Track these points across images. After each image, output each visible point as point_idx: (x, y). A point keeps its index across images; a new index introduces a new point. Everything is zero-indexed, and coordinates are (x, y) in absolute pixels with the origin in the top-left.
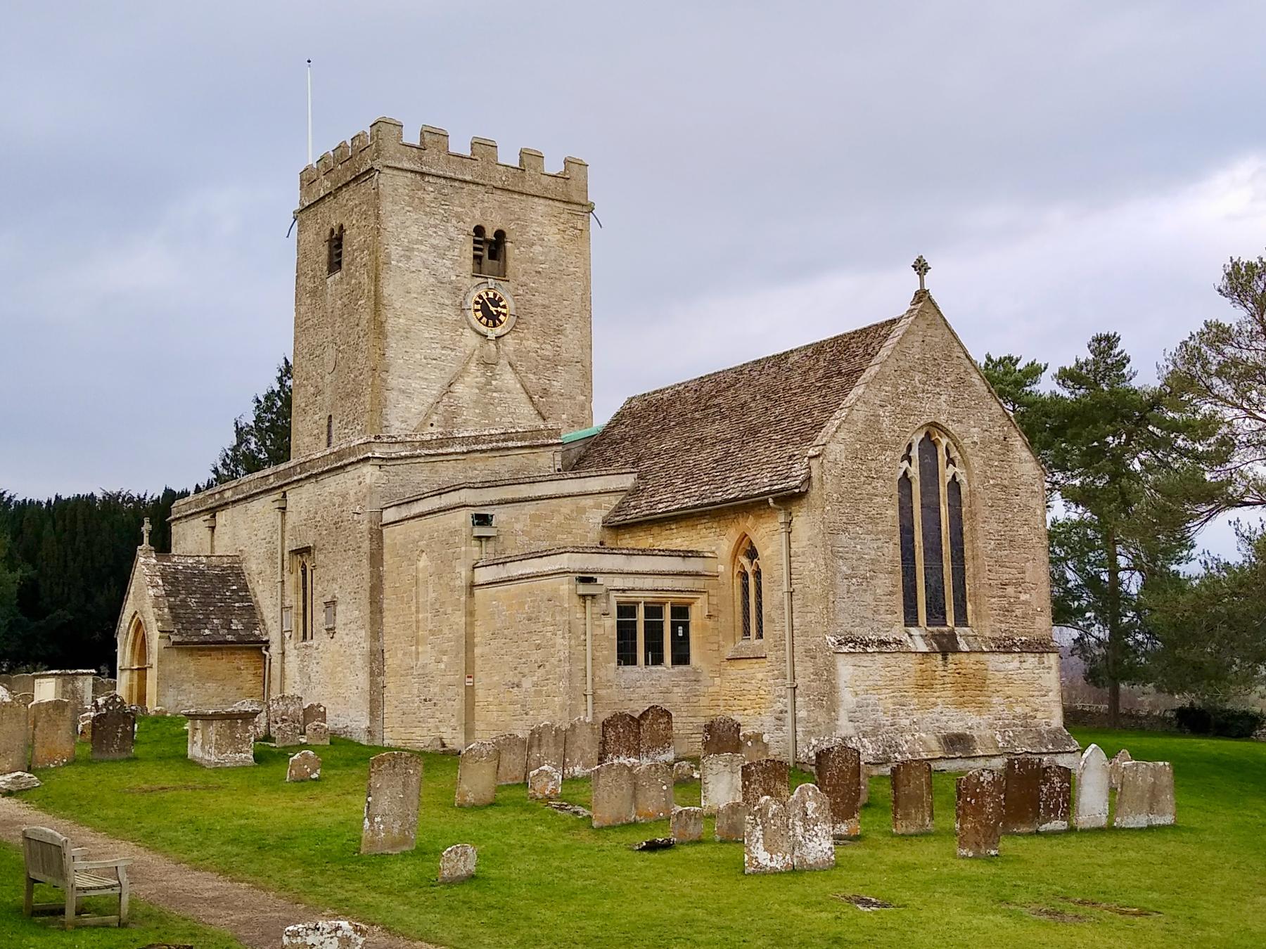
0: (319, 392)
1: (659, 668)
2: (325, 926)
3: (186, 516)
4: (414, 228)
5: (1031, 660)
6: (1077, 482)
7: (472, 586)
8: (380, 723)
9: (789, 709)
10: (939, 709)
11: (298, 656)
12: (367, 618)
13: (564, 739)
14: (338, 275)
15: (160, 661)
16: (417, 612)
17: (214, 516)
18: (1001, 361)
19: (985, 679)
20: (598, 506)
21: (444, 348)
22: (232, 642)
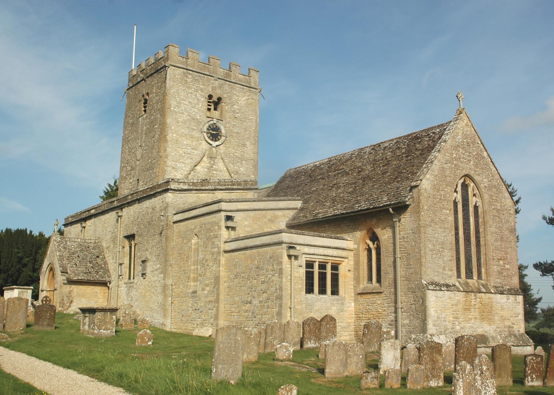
0: (133, 169)
5: (512, 297)
20: (284, 216)
21: (192, 149)
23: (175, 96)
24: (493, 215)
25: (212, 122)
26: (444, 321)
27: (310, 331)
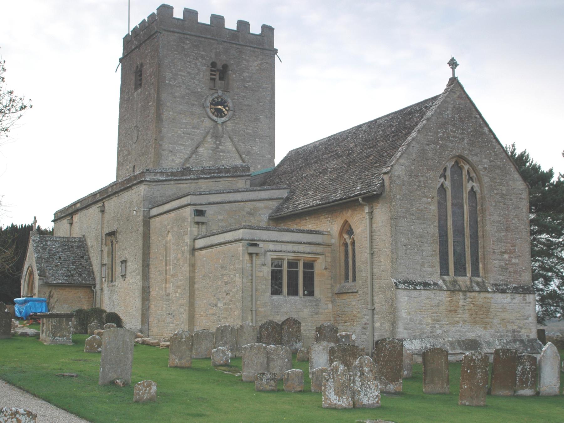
0: (129, 154)
5: (518, 297)
7: (194, 250)
9: (370, 322)
12: (141, 269)
13: (236, 333)
14: (139, 90)
15: (39, 292)
17: (72, 218)
20: (267, 208)
21: (193, 128)
23: (171, 66)
24: (495, 201)
25: (216, 95)
26: (419, 324)
27: (269, 335)
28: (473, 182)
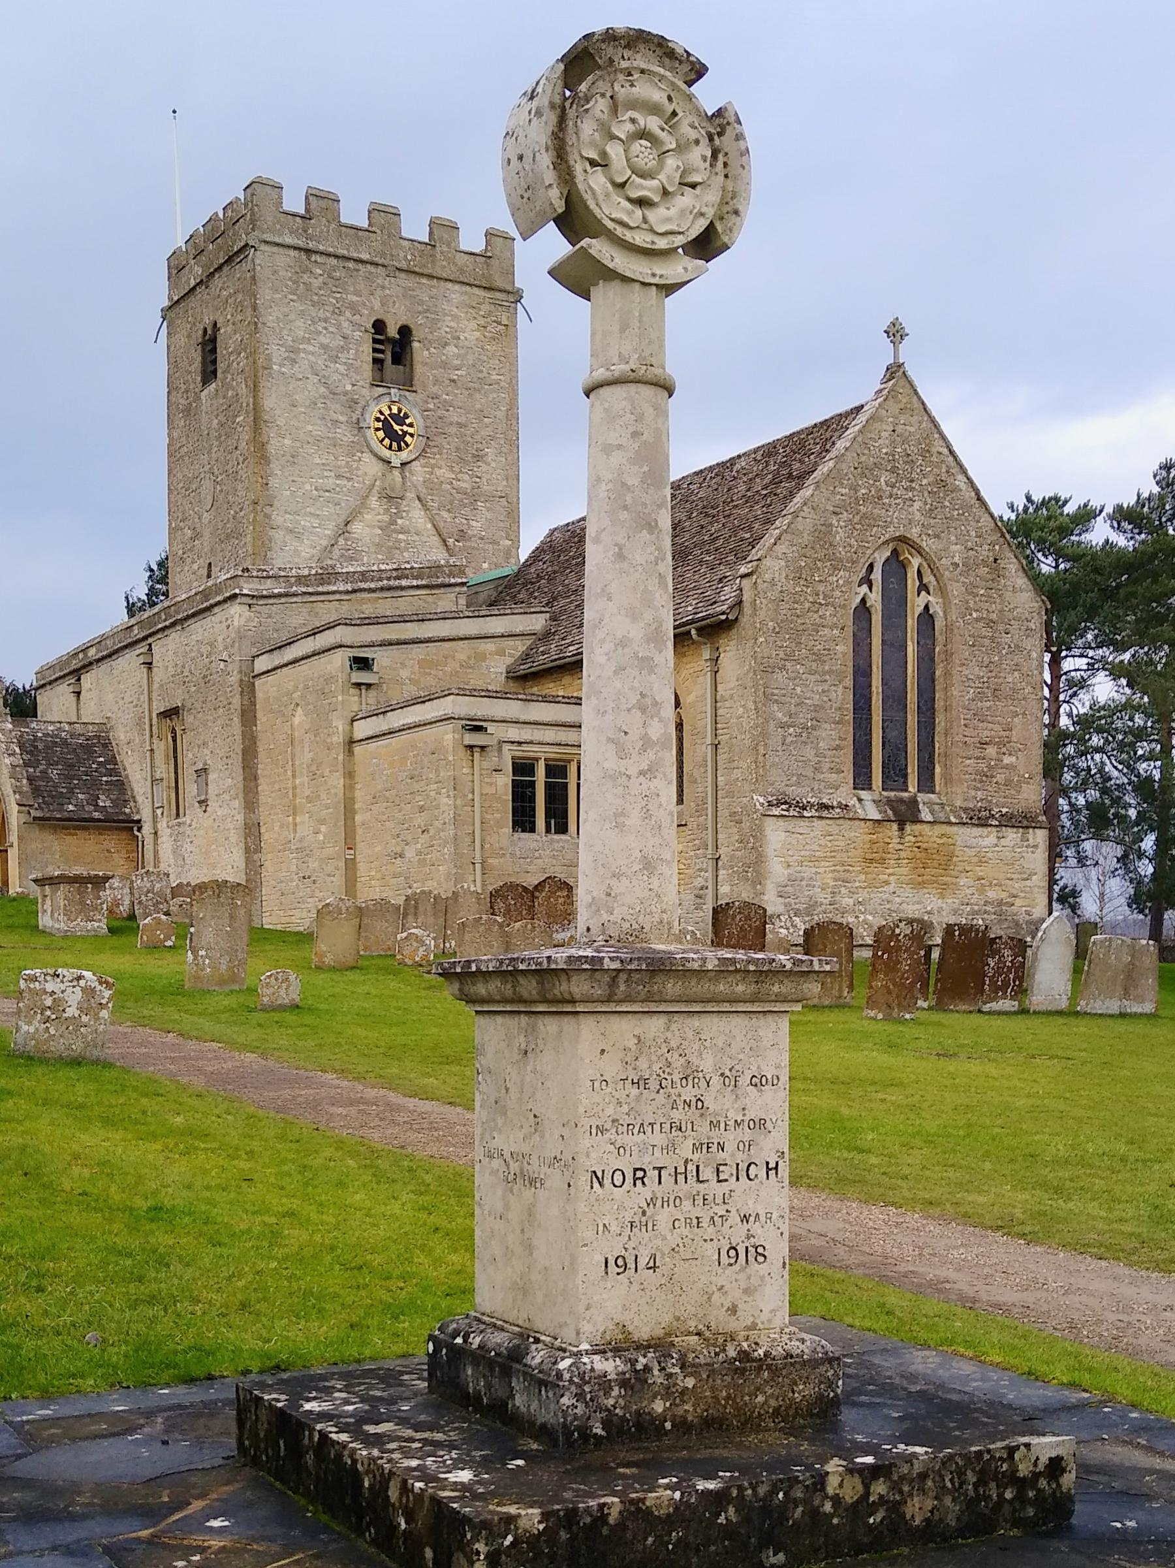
0: (196, 536)
1: (563, 837)
2: (66, 973)
3: (50, 683)
4: (299, 323)
5: (1012, 836)
6: (1127, 656)
7: (351, 742)
8: (258, 902)
9: (710, 884)
10: (891, 888)
11: (171, 836)
16: (294, 776)
17: (79, 680)
18: (1044, 503)
19: (951, 856)
20: (501, 653)
21: (338, 477)
22: (99, 820)
28: (929, 593)
